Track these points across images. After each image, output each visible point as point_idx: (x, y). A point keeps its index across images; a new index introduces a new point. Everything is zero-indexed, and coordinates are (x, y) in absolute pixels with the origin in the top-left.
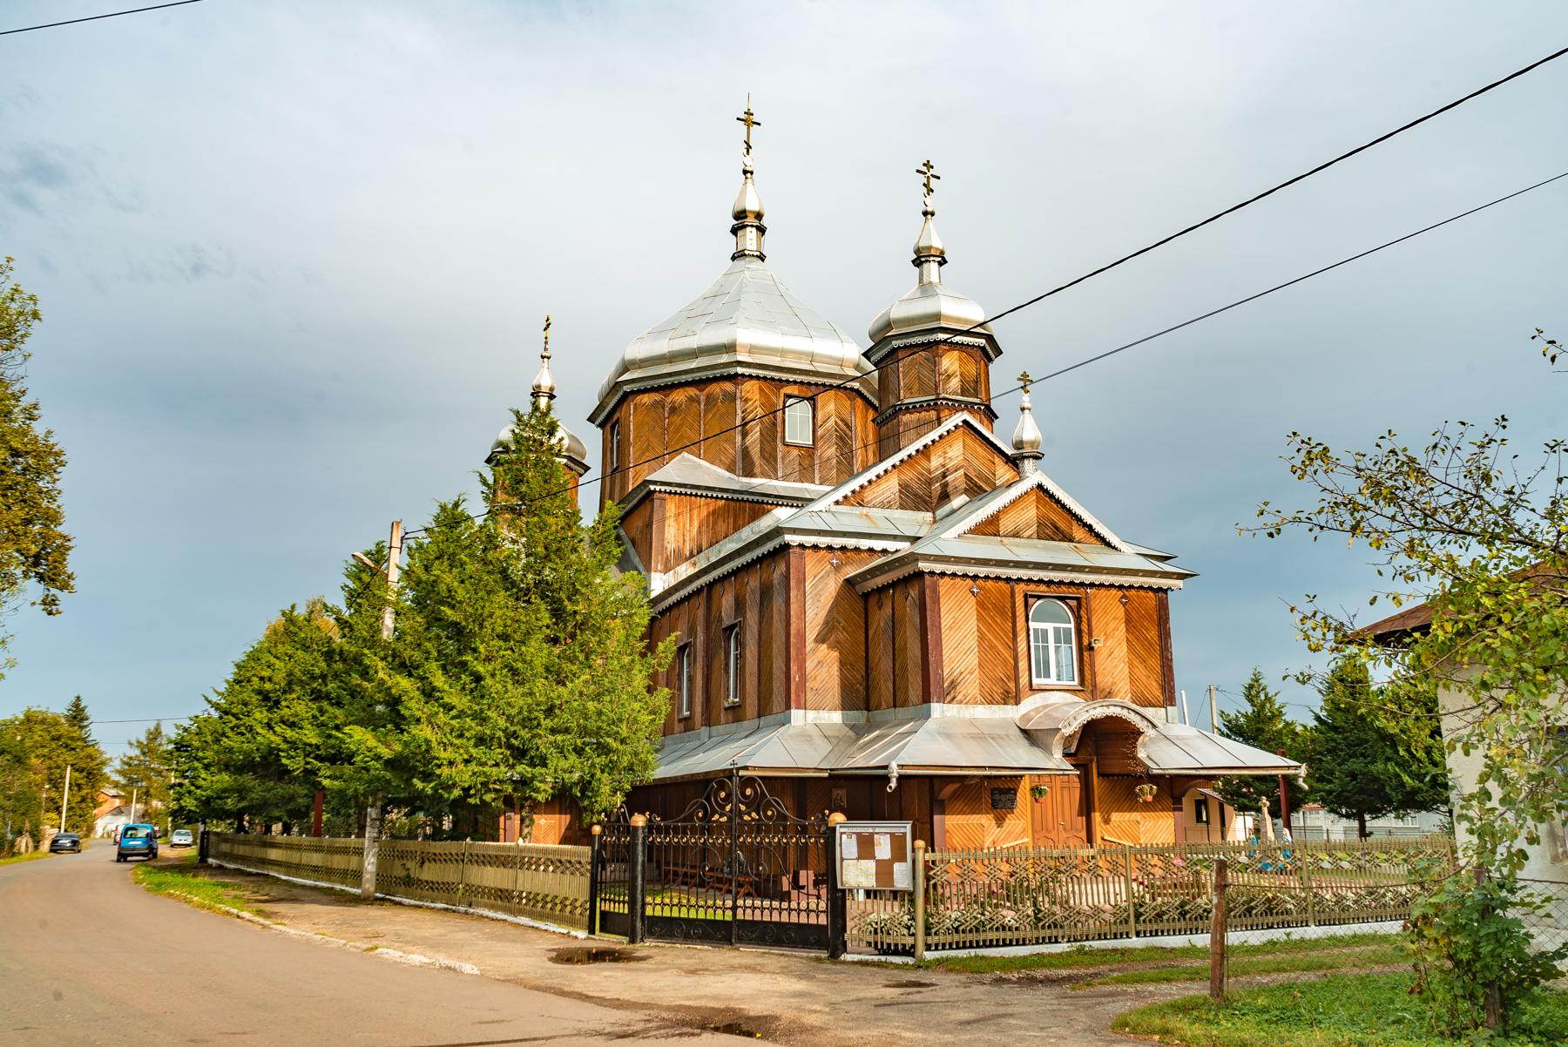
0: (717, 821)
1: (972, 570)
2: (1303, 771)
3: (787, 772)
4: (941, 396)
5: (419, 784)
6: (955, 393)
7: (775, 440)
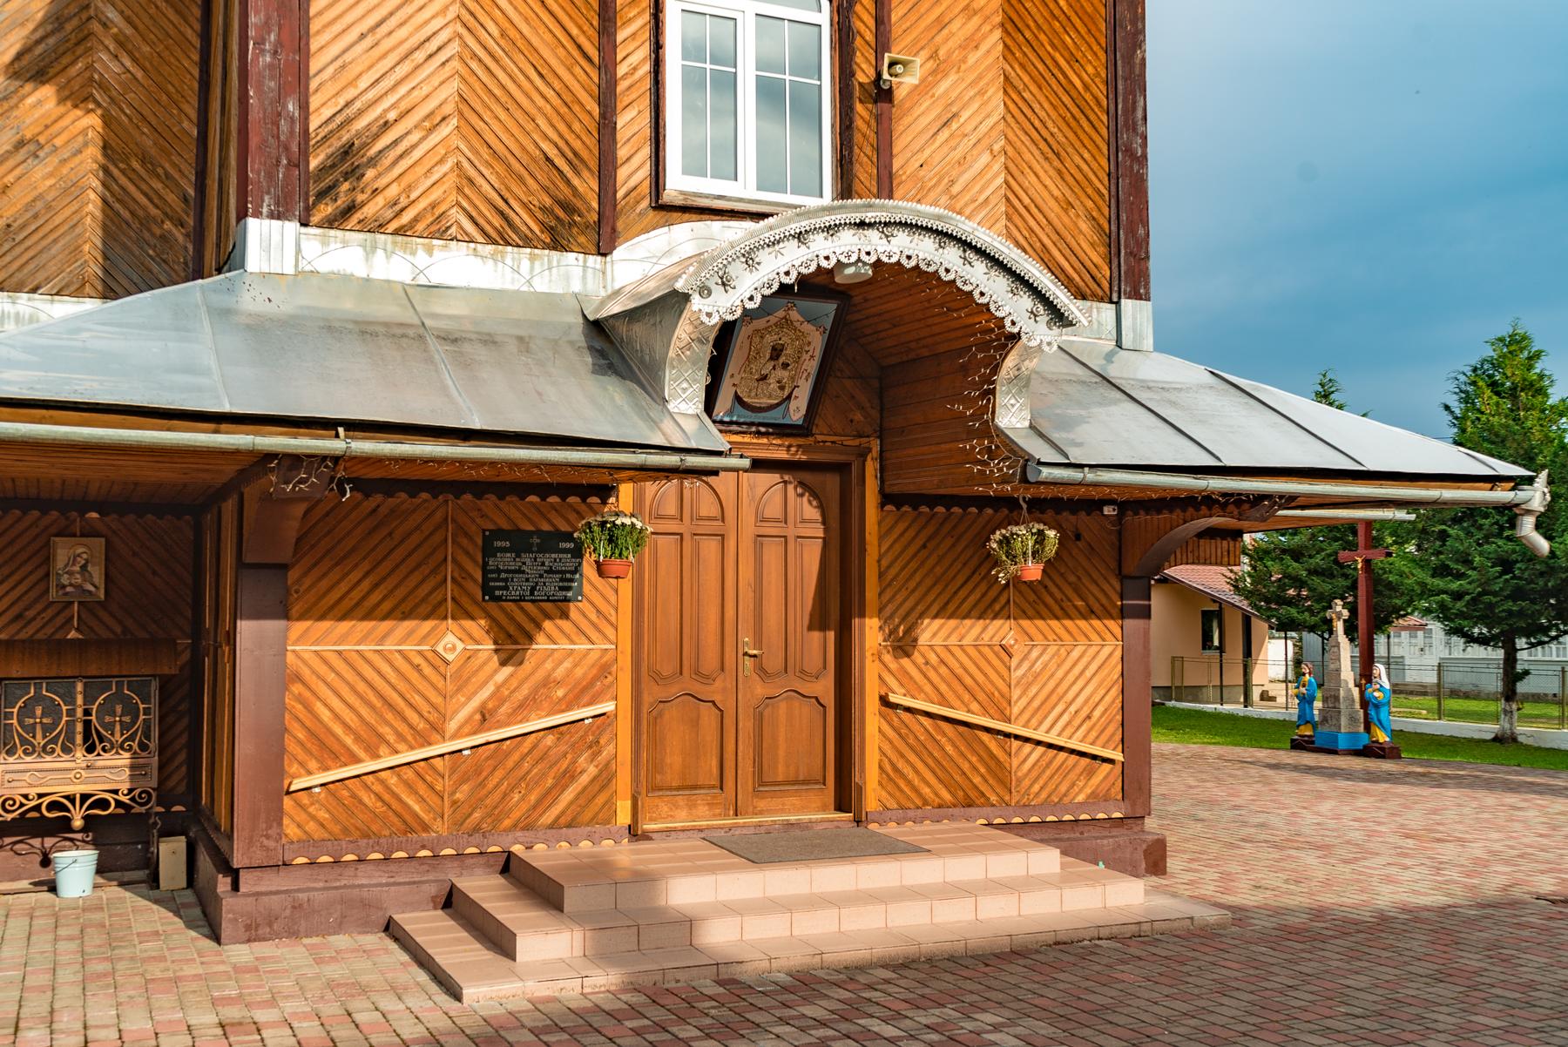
2: (1537, 496)
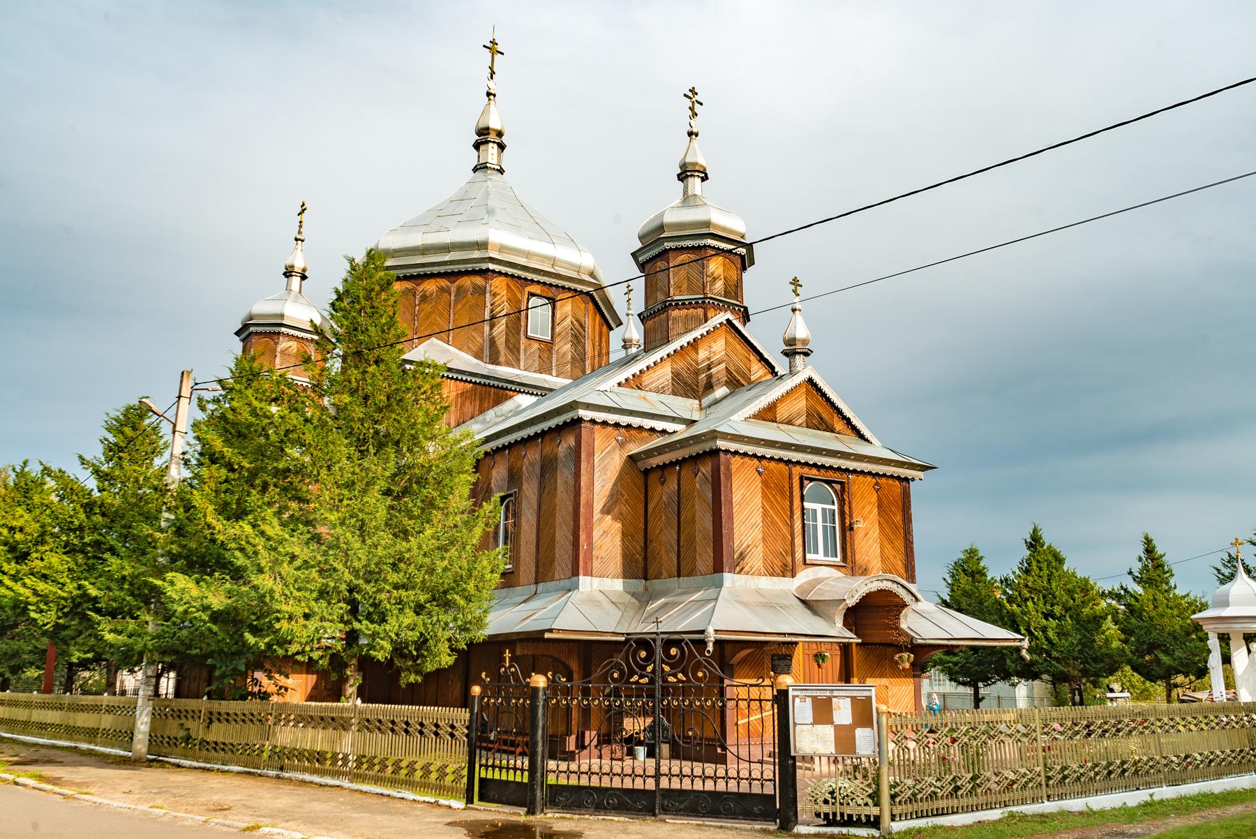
0: (637, 683)
1: (760, 451)
2: (1026, 644)
3: (588, 635)
4: (709, 295)
5: (250, 639)
6: (719, 294)
7: (518, 333)
